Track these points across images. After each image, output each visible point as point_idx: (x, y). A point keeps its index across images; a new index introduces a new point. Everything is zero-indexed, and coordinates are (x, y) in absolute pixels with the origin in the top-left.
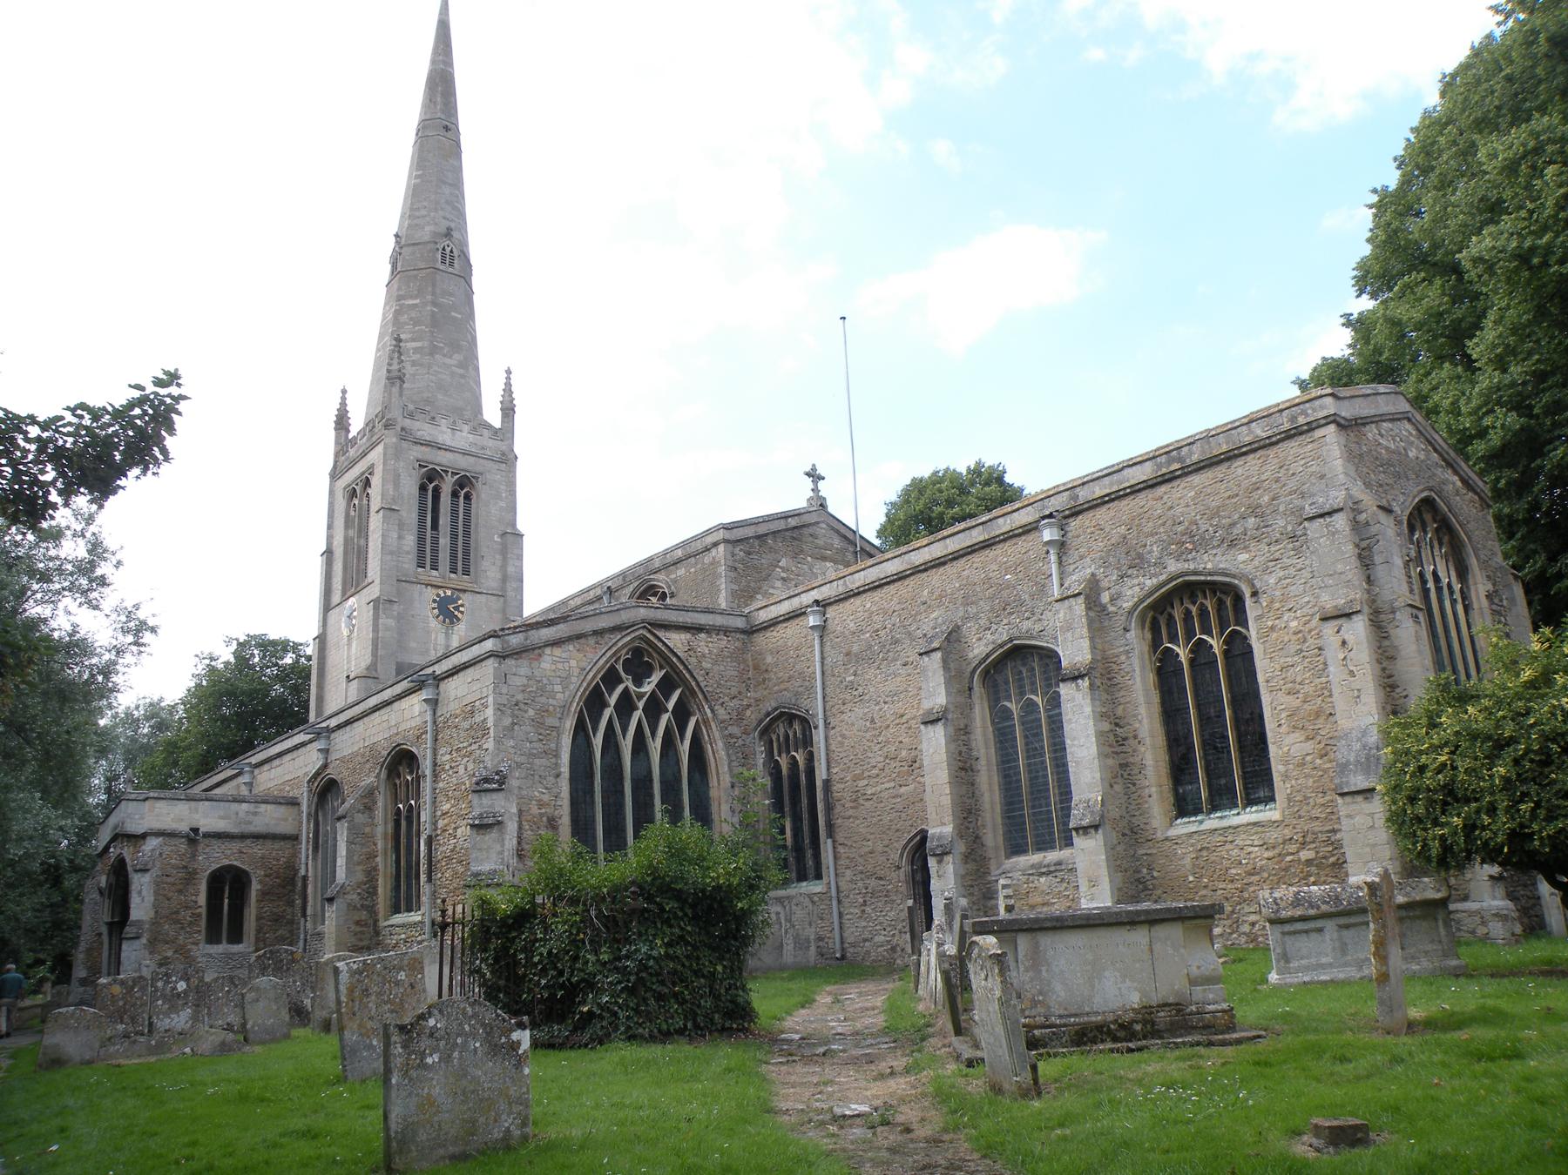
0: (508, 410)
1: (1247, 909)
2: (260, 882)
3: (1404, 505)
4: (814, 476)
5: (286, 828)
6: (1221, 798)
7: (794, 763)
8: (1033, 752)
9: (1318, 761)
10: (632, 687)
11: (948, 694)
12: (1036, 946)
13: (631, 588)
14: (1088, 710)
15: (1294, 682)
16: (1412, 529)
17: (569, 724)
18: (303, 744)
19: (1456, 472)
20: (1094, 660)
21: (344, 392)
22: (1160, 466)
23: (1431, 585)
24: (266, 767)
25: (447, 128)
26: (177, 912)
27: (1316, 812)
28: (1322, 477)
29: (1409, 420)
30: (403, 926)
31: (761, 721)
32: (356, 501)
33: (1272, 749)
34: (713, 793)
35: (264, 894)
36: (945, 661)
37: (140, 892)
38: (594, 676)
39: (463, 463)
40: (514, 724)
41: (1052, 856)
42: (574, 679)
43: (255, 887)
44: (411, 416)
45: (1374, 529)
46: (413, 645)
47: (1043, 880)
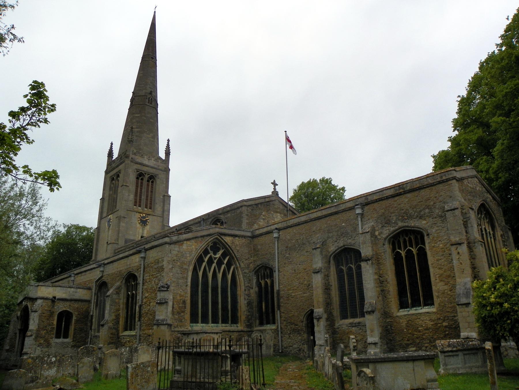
0: (168, 153)
1: (424, 342)
2: (76, 317)
3: (476, 206)
4: (274, 184)
5: (87, 298)
6: (416, 303)
7: (266, 283)
8: (351, 284)
9: (449, 292)
10: (213, 256)
11: (322, 263)
12: (376, 367)
13: (211, 220)
14: (371, 271)
15: (441, 265)
16: (478, 214)
17: (191, 268)
18: (94, 268)
19: (490, 194)
20: (373, 255)
21: (112, 144)
22: (396, 190)
23: (484, 232)
24: (80, 275)
25: (152, 58)
26: (46, 327)
27: (448, 310)
28: (451, 197)
29: (476, 177)
30: (128, 336)
31: (255, 268)
32: (114, 182)
33: (434, 288)
34: (239, 293)
35: (77, 321)
36: (321, 252)
37: (33, 319)
38: (200, 251)
39: (152, 171)
40: (172, 267)
41: (357, 320)
42: (193, 252)
43: (74, 318)
44: (135, 154)
45: (468, 215)
46: (131, 232)
47: (353, 328)
